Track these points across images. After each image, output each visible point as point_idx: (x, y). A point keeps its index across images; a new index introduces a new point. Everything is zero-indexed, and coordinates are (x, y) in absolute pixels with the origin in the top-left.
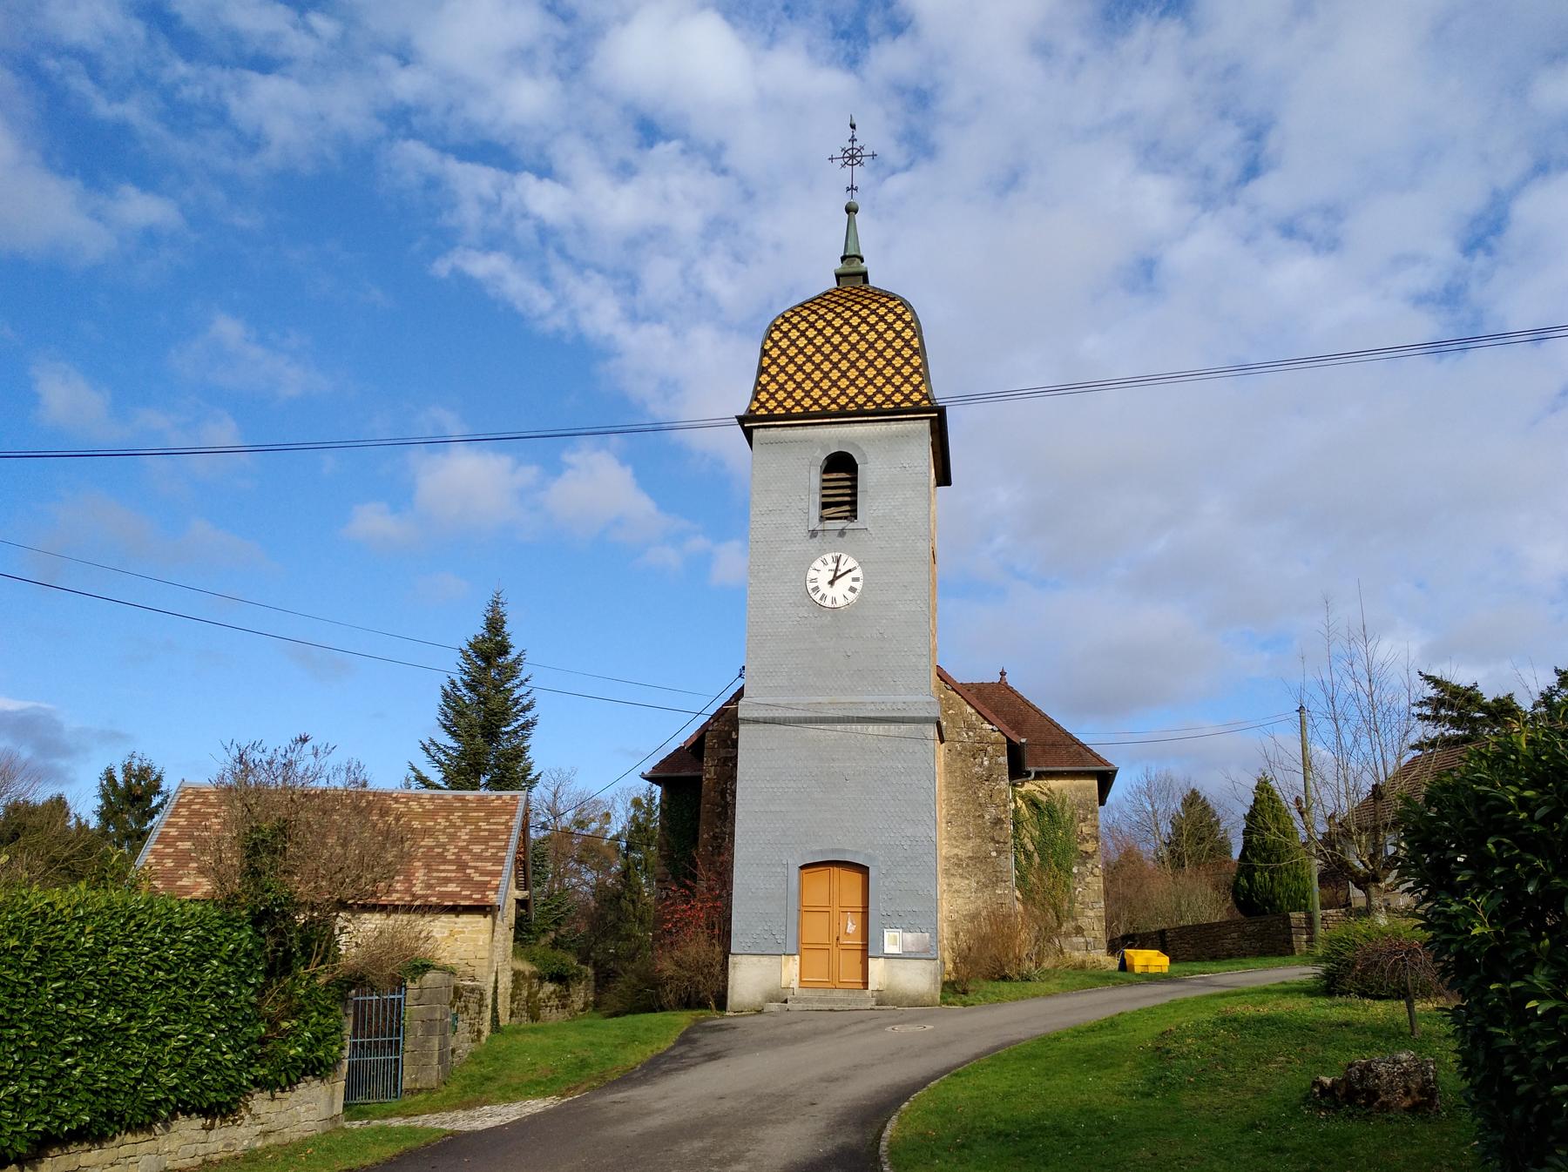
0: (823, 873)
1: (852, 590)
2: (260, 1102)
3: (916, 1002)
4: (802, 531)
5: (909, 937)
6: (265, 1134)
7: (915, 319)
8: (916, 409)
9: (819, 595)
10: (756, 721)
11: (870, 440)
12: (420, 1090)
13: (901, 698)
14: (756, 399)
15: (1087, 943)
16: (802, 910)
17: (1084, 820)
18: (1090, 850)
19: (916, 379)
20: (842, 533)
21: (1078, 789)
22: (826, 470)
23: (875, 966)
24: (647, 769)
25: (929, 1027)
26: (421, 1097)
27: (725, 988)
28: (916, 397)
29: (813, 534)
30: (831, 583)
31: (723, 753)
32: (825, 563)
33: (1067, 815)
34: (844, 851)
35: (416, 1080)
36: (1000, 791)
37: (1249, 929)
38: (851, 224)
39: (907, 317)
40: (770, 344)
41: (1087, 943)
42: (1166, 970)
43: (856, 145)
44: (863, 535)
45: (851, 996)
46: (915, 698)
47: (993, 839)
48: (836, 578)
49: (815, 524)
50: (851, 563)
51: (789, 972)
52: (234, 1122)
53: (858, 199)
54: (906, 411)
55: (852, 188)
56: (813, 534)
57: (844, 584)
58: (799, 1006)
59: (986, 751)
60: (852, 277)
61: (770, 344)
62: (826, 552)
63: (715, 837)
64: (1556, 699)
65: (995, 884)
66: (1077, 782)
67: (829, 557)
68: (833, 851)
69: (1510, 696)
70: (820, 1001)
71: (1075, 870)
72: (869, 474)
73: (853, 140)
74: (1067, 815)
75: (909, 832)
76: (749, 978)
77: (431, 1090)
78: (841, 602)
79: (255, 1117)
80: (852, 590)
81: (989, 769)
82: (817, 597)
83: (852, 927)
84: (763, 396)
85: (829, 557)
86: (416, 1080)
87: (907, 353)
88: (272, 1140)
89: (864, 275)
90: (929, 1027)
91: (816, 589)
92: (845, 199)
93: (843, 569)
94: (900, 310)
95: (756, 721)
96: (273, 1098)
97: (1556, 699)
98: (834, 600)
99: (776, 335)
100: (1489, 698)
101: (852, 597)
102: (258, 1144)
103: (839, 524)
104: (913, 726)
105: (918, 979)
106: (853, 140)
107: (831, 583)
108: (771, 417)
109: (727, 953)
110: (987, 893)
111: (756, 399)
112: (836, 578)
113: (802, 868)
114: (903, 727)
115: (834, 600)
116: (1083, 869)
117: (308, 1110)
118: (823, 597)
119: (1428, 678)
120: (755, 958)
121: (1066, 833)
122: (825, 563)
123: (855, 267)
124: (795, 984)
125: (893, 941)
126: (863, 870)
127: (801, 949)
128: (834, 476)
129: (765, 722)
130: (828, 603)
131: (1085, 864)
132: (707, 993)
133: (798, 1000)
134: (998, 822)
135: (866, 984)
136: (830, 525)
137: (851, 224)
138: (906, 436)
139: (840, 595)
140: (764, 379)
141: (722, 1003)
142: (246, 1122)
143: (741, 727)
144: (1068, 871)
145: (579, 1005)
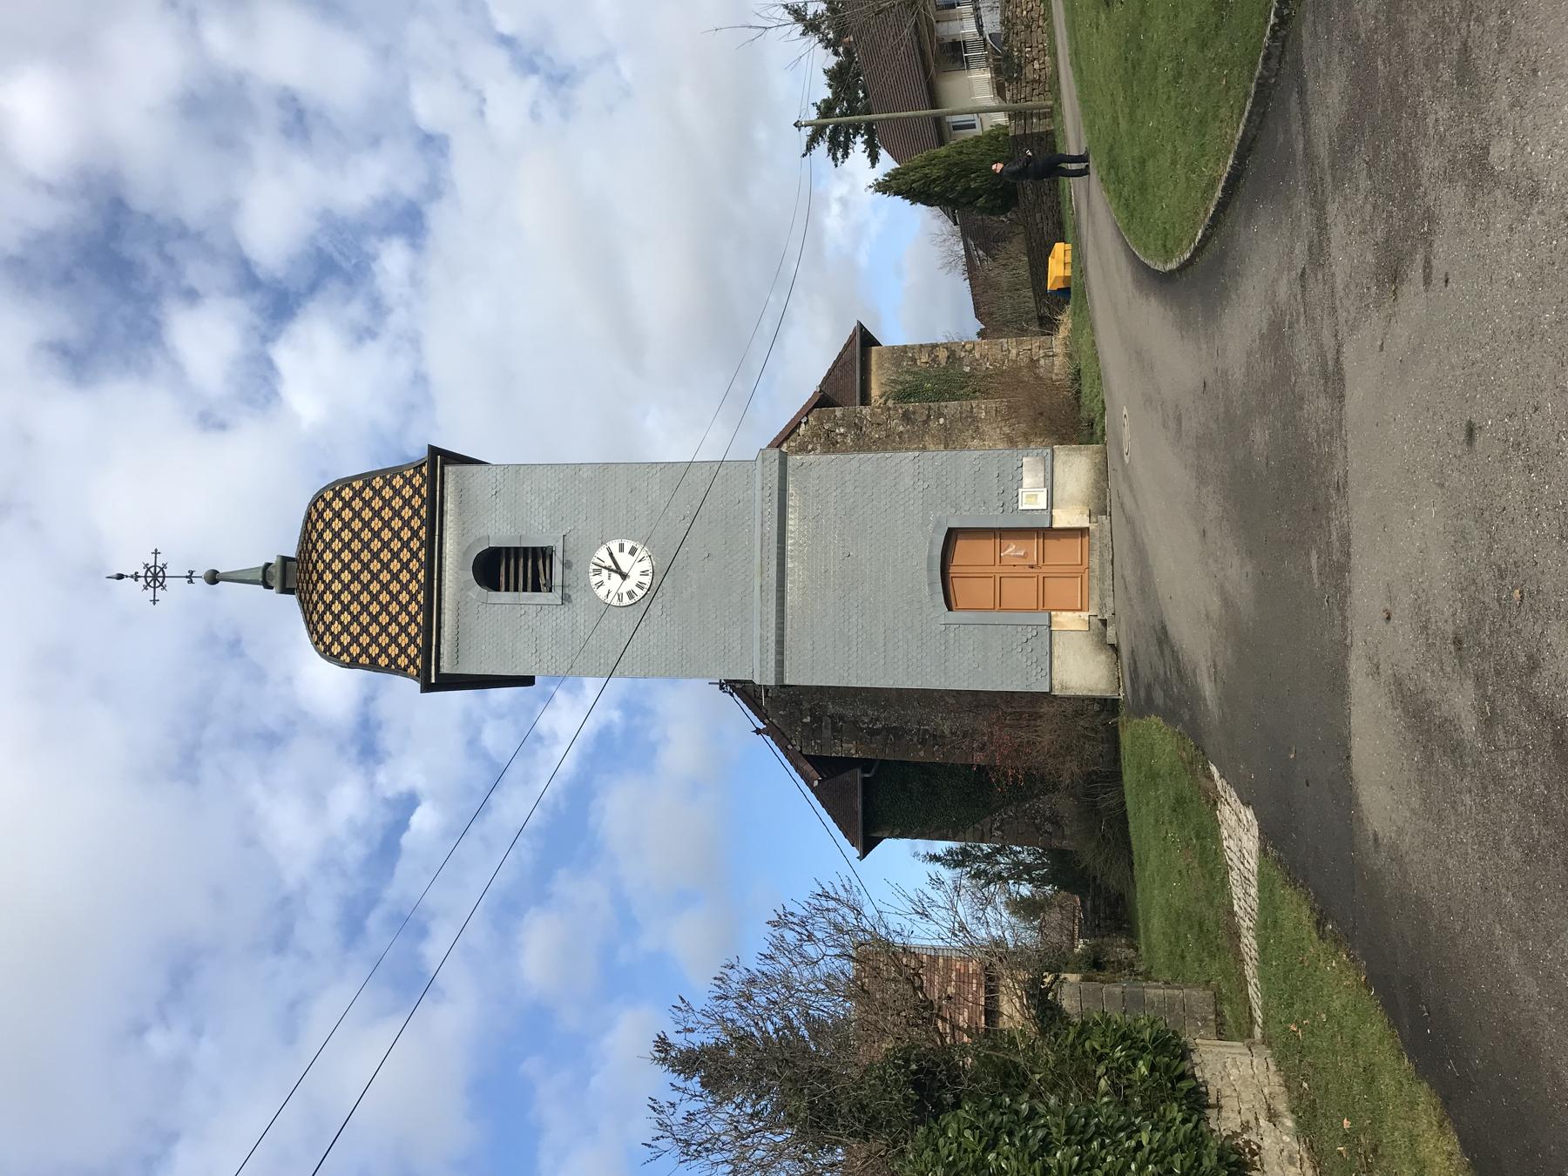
0: (957, 585)
1: (633, 551)
2: (1226, 1122)
3: (1102, 473)
4: (562, 612)
5: (1027, 481)
6: (1273, 1116)
7: (331, 487)
8: (431, 480)
9: (637, 591)
10: (780, 664)
11: (463, 532)
12: (1218, 1014)
13: (758, 493)
14: (405, 669)
15: (1046, 356)
16: (999, 605)
17: (914, 360)
18: (946, 353)
19: (398, 482)
20: (566, 565)
21: (880, 367)
22: (495, 587)
23: (1062, 519)
24: (855, 852)
25: (1125, 412)
26: (1226, 1009)
27: (1093, 699)
28: (417, 481)
29: (566, 598)
30: (624, 576)
31: (827, 733)
32: (601, 584)
33: (909, 378)
34: (930, 558)
35: (1204, 1019)
36: (873, 414)
37: (1031, 197)
38: (232, 578)
39: (329, 495)
40: (345, 658)
41: (1046, 356)
42: (1069, 246)
43: (142, 573)
44: (571, 540)
45: (1097, 546)
46: (758, 478)
47: (926, 422)
48: (618, 571)
49: (555, 596)
50: (602, 553)
51: (1070, 622)
52: (1253, 1153)
53: (201, 571)
54: (432, 491)
55: (190, 577)
56: (566, 598)
57: (625, 561)
58: (1109, 601)
59: (830, 431)
60: (288, 576)
61: (345, 658)
62: (588, 584)
63: (923, 742)
64: (831, 36)
65: (975, 419)
66: (874, 367)
67: (595, 580)
68: (930, 570)
69: (825, 72)
70: (1102, 580)
71: (967, 369)
72: (501, 533)
73: (136, 577)
74: (909, 378)
75: (908, 481)
76: (1080, 670)
77: (1218, 999)
78: (646, 565)
79: (1246, 1127)
80: (633, 551)
81: (848, 427)
82: (640, 593)
83: (1012, 549)
84: (403, 661)
85: (595, 580)
86: (1204, 1019)
87: (368, 494)
88: (1281, 1106)
89: (285, 560)
90: (1125, 412)
91: (631, 594)
92: (200, 583)
93: (609, 563)
94: (321, 505)
95: (780, 664)
96: (1219, 1107)
97: (831, 36)
98: (644, 573)
99: (336, 649)
100: (828, 93)
101: (642, 552)
102: (1289, 1123)
103: (557, 567)
104: (790, 478)
105: (1075, 469)
106: (136, 577)
107: (624, 576)
108: (425, 651)
109: (1047, 696)
110: (984, 427)
111: (405, 669)
112: (618, 571)
113: (950, 609)
114: (791, 490)
115: (644, 573)
116: (966, 361)
117: (1235, 1065)
118: (640, 585)
119: (809, 149)
120: (1056, 663)
121: (928, 379)
122: (601, 584)
123: (276, 572)
124: (1085, 615)
125: (1032, 498)
126: (952, 535)
127: (1043, 605)
128: (503, 579)
129: (780, 651)
130: (647, 580)
131: (961, 359)
132: (1101, 712)
133: (1102, 606)
134: (907, 418)
135: (1082, 532)
136: (557, 580)
137: (232, 578)
138: (461, 492)
139: (638, 568)
140: (383, 661)
141: (1108, 706)
142: (1254, 1138)
143: (787, 682)
144: (969, 376)
145: (1131, 953)
